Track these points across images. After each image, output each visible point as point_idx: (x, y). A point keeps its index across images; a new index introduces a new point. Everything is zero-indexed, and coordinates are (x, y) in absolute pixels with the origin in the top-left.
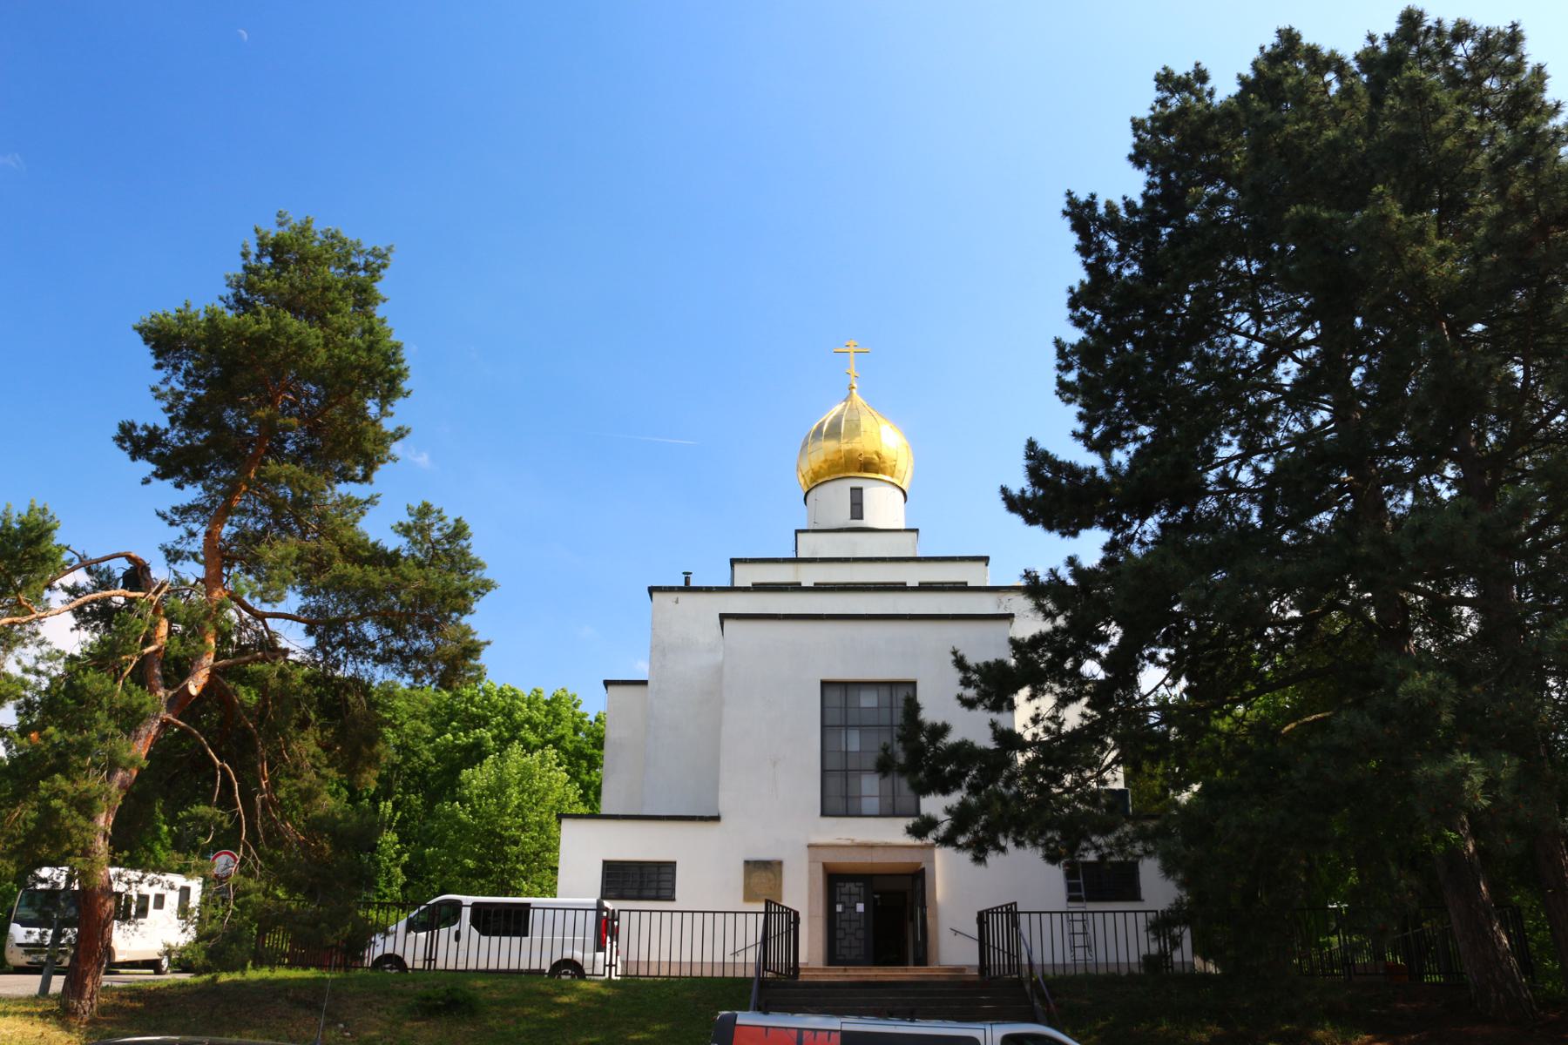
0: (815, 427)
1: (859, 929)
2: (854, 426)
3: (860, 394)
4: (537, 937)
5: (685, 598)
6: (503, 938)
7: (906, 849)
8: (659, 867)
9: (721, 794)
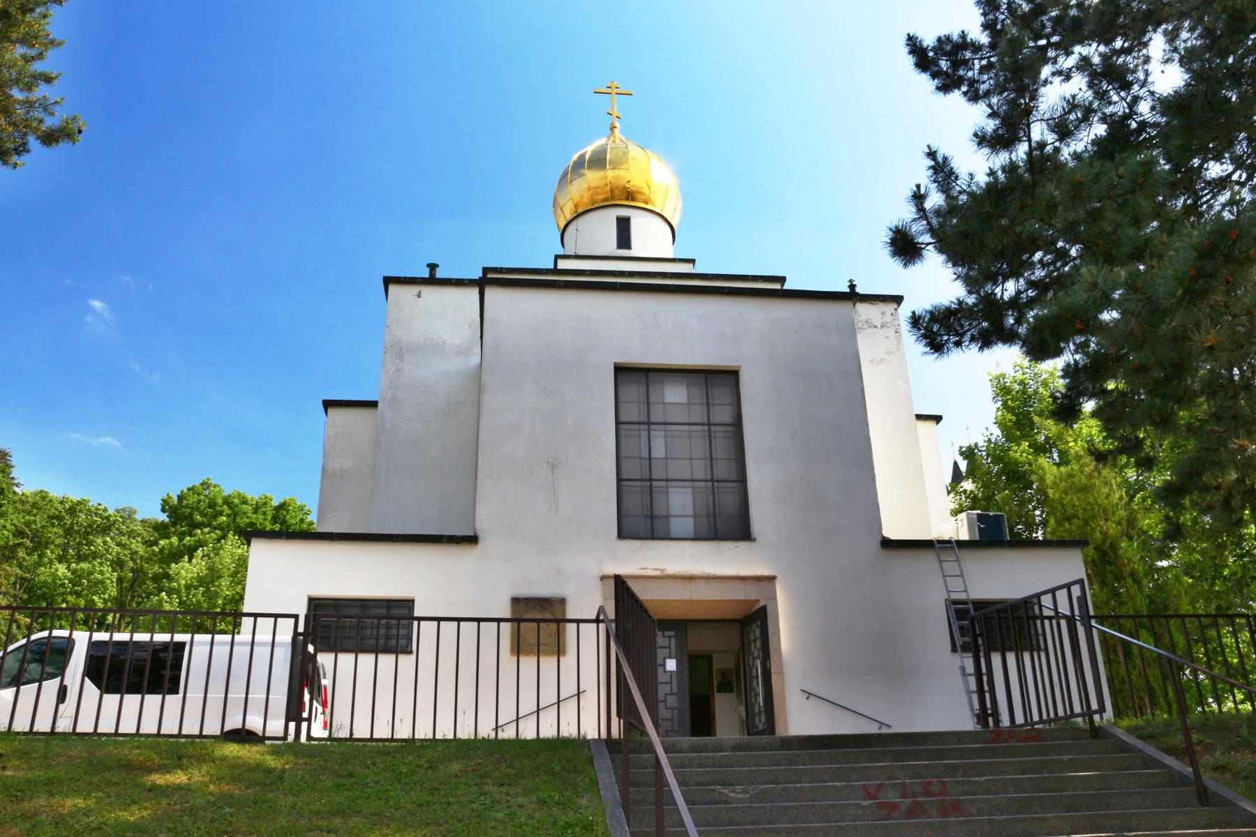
0: (575, 157)
1: (672, 694)
2: (621, 153)
3: (621, 131)
4: (195, 695)
5: (429, 292)
6: (127, 697)
7: (739, 582)
8: (388, 608)
9: (479, 507)
